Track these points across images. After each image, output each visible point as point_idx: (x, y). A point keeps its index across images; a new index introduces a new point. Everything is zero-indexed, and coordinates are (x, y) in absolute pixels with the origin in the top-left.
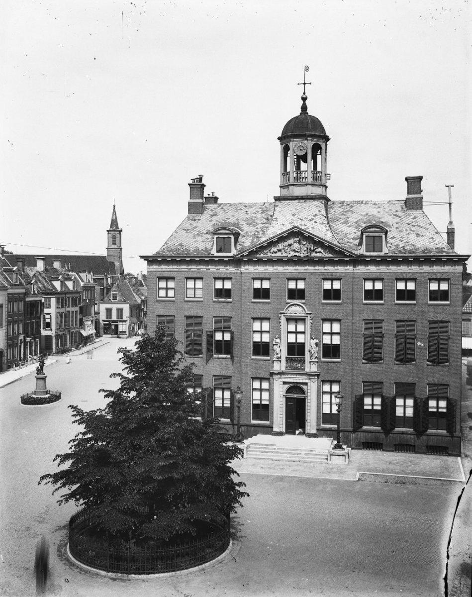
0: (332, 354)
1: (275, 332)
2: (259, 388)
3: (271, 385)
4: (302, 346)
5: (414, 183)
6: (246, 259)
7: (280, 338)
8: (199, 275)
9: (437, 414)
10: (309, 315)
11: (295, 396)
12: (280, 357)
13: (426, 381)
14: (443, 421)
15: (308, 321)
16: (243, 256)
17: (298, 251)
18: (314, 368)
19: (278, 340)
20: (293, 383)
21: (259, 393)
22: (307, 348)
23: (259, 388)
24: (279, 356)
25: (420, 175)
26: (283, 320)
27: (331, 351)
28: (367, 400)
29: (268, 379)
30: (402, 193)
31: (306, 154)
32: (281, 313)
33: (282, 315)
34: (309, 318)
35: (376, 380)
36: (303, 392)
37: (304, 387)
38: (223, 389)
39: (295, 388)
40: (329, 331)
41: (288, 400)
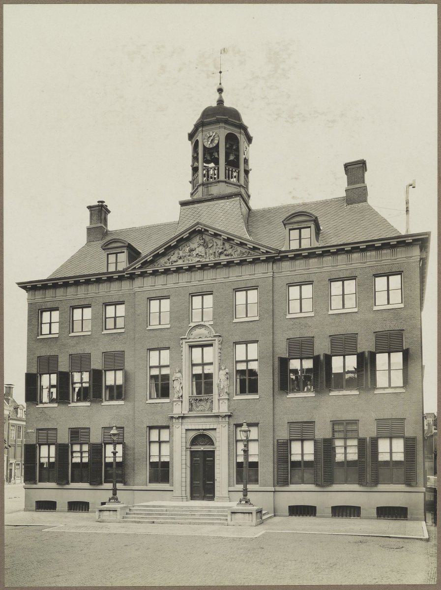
0: (247, 389)
1: (176, 358)
2: (117, 316)
3: (171, 435)
4: (209, 376)
5: (356, 170)
6: (138, 272)
7: (180, 371)
8: (86, 303)
9: (391, 464)
10: (216, 339)
11: (202, 448)
12: (182, 396)
13: (374, 416)
14: (400, 472)
15: (216, 344)
16: (135, 269)
17: (202, 255)
18: (224, 409)
19: (179, 375)
20: (199, 430)
21: (157, 445)
22: (215, 381)
23: (117, 316)
24: (180, 395)
25: (362, 158)
26: (185, 348)
27: (248, 382)
28: (296, 447)
29: (167, 427)
30: (339, 187)
31: (218, 145)
32: (182, 339)
33: (184, 341)
34: (217, 342)
35: (305, 420)
36: (210, 442)
37: (210, 434)
38: (115, 444)
39: (202, 438)
40: (244, 359)
41: (193, 454)
